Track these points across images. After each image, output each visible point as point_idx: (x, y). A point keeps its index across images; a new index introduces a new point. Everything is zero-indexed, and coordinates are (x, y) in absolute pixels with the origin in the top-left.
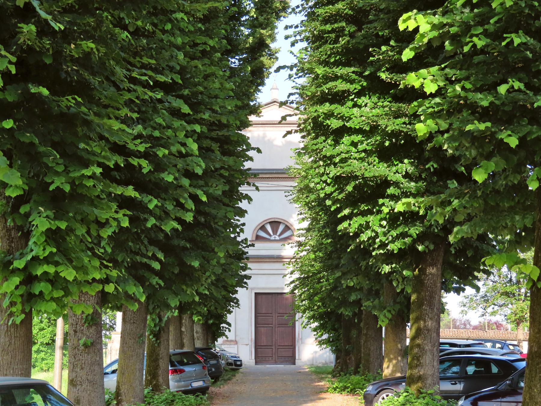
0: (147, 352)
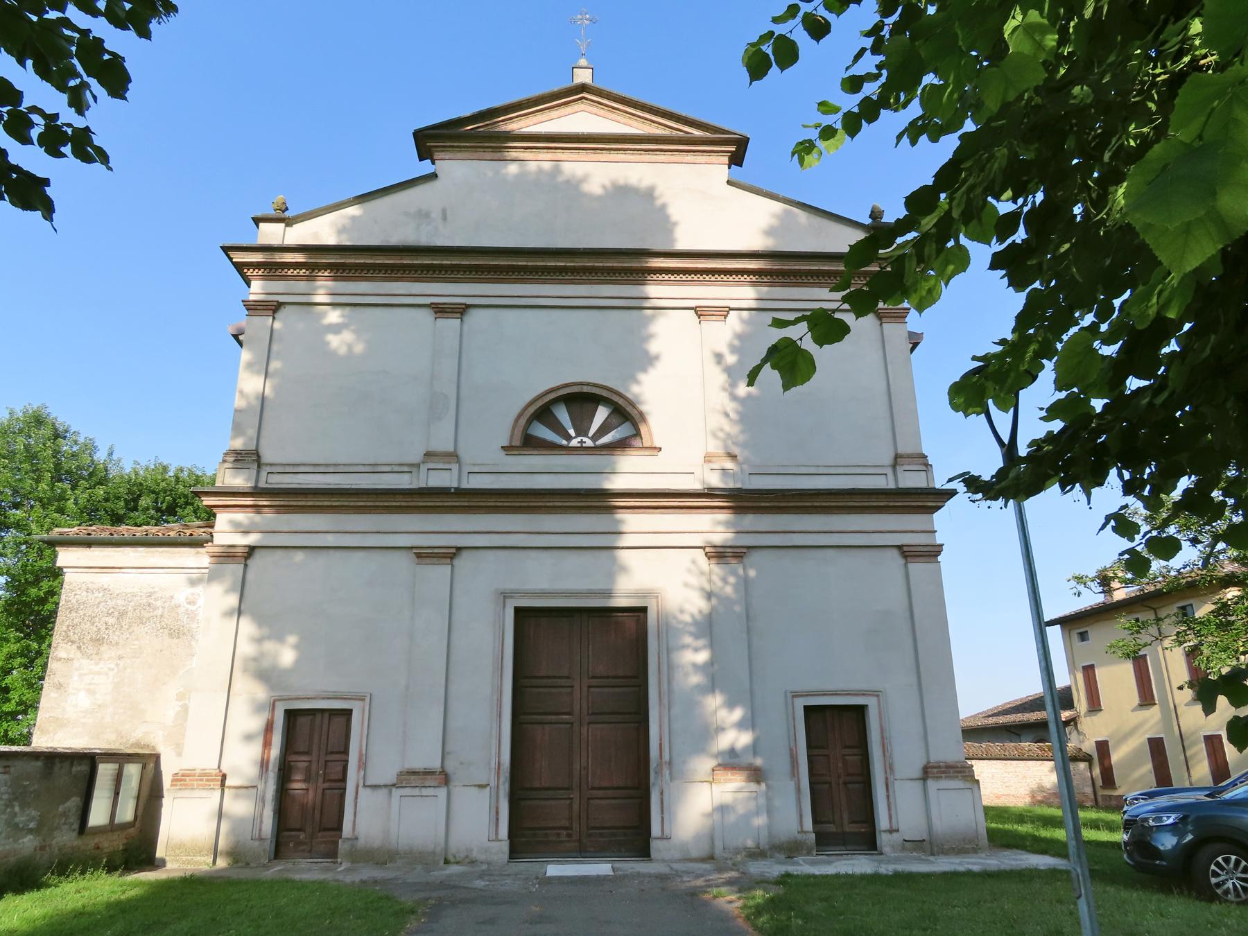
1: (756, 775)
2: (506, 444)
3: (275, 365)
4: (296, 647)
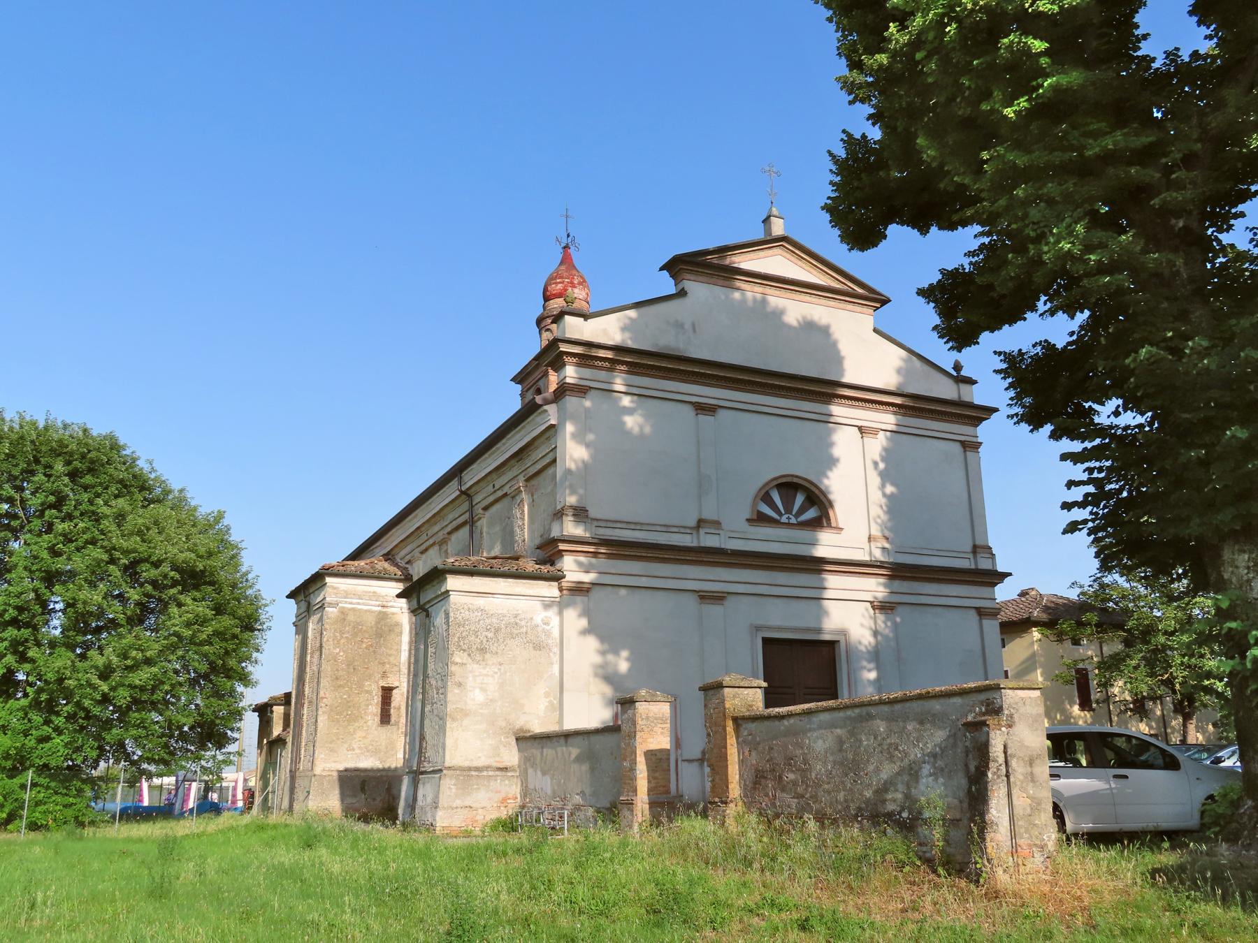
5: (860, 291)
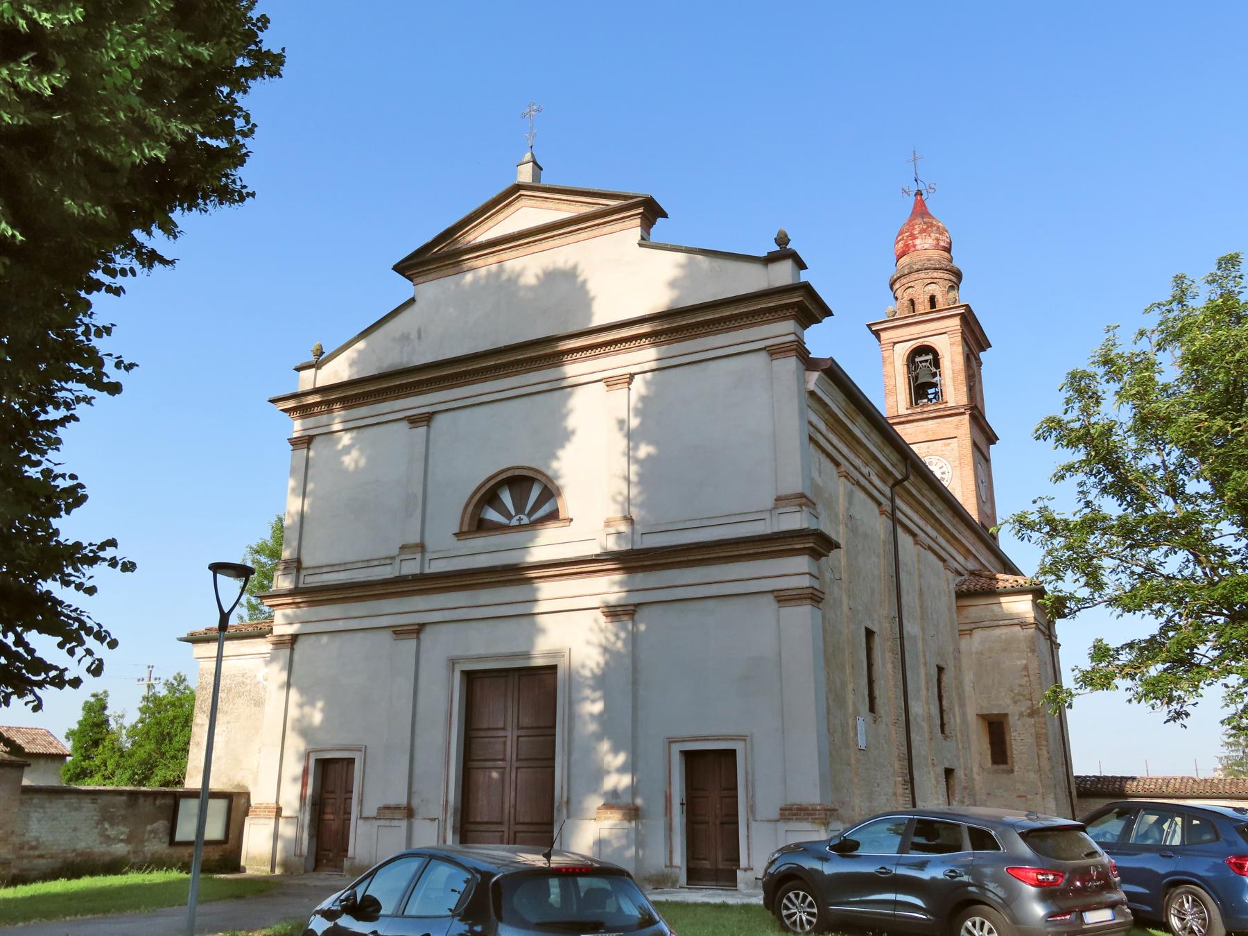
0: (158, 881)
1: (633, 813)
2: (457, 531)
3: (310, 486)
4: (322, 710)
5: (613, 203)
